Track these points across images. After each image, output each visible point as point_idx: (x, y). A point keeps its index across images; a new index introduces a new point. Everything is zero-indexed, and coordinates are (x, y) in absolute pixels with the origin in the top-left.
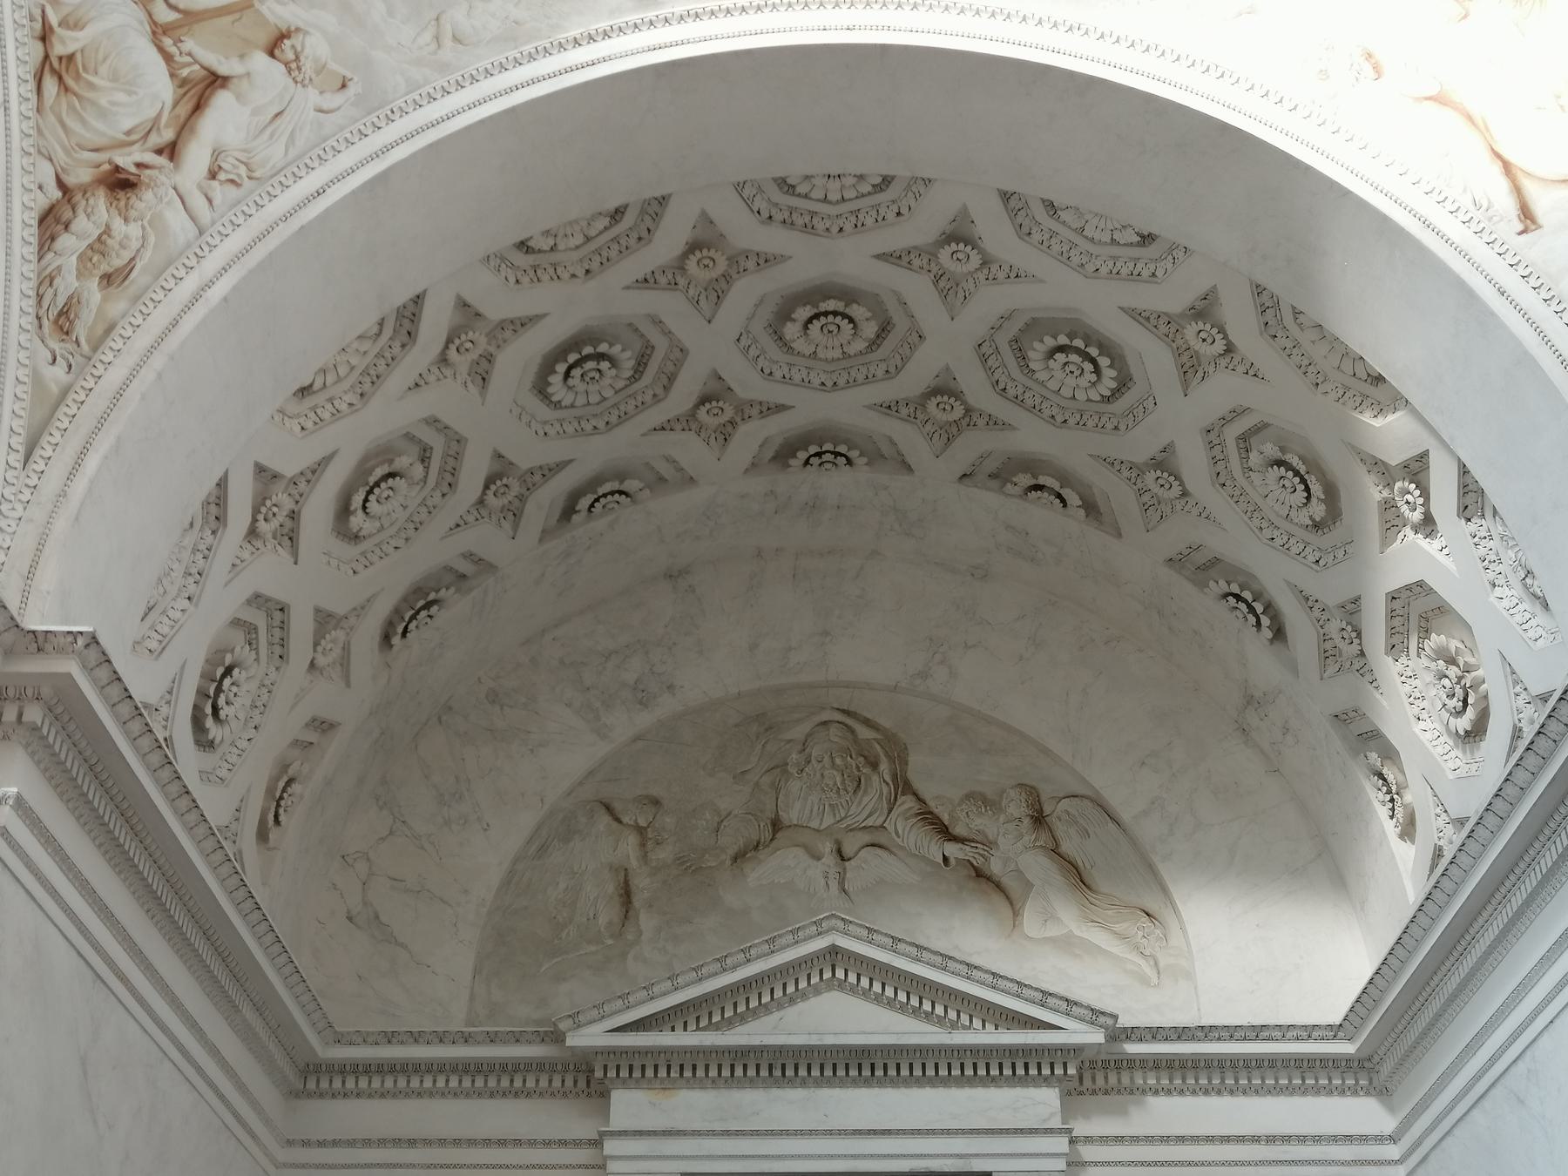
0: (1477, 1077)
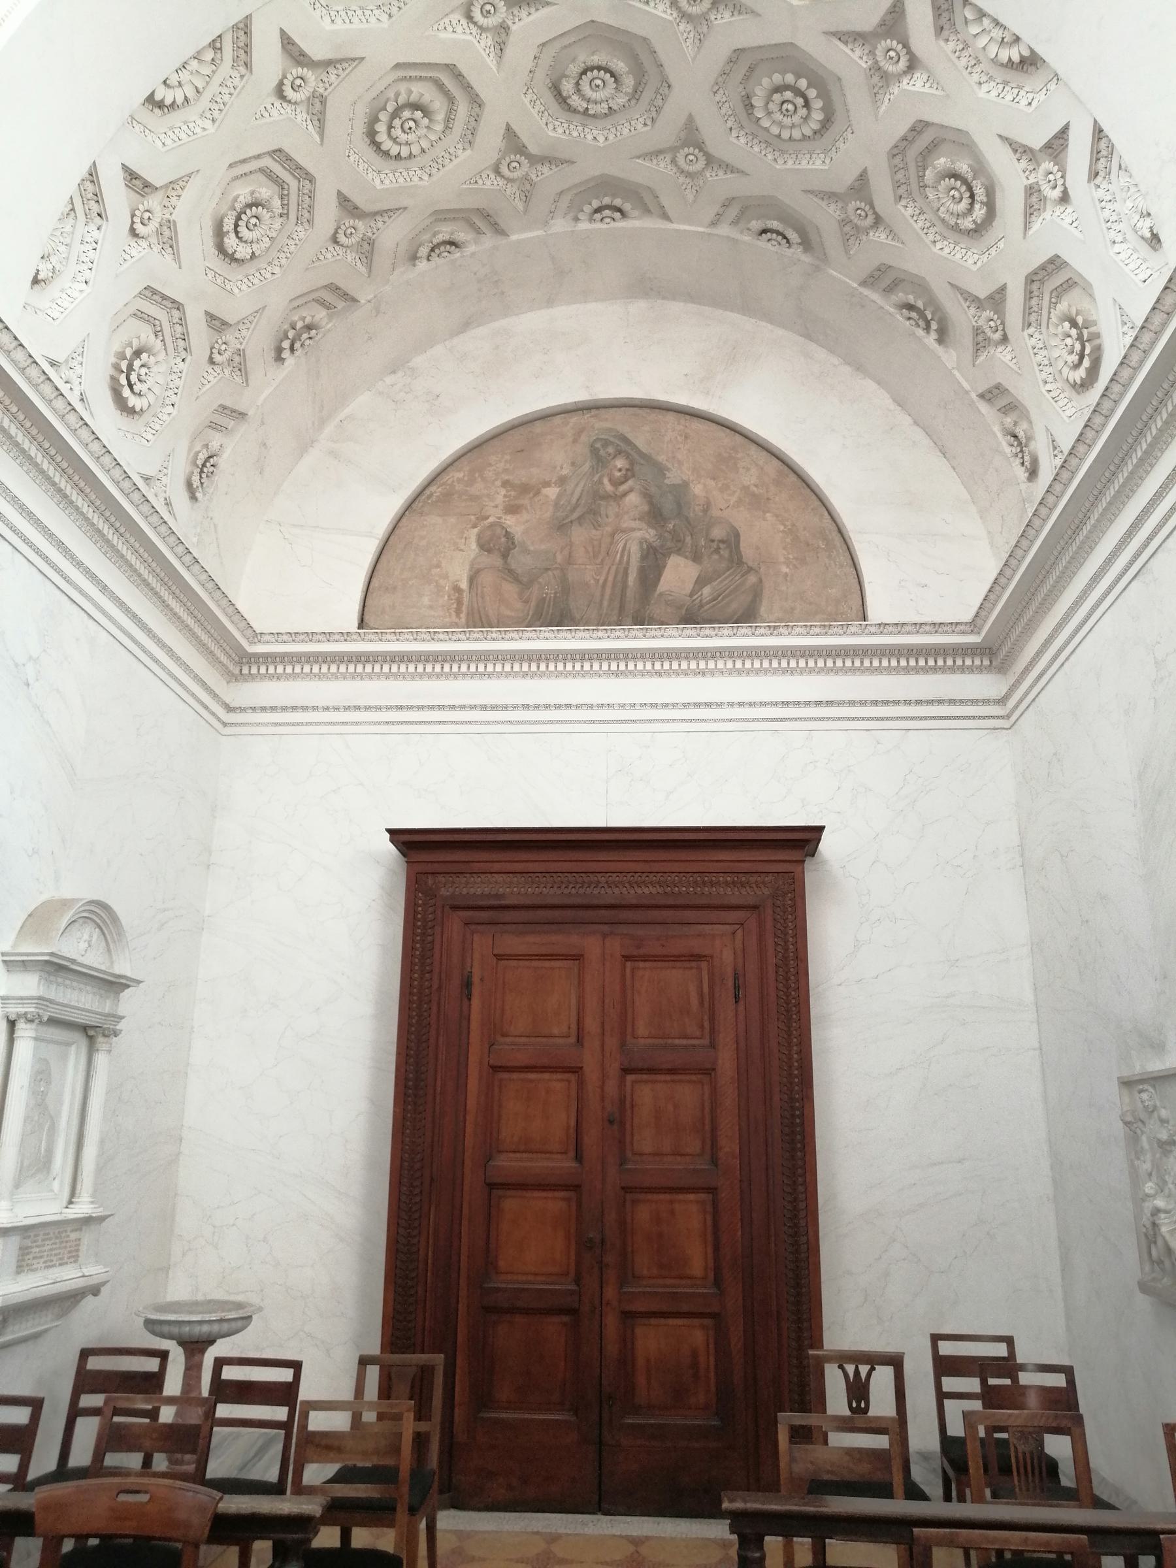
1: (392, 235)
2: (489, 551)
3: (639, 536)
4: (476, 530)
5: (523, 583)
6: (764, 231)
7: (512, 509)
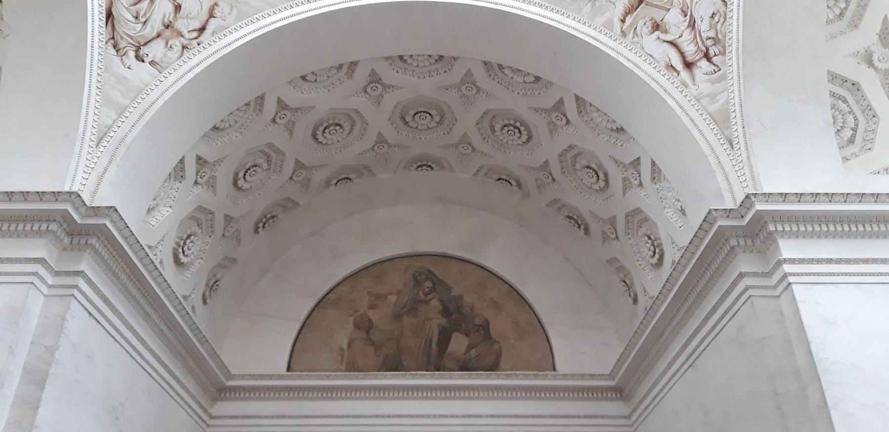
1: (318, 177)
2: (359, 329)
3: (436, 322)
4: (352, 318)
5: (377, 347)
6: (500, 179)
7: (372, 307)
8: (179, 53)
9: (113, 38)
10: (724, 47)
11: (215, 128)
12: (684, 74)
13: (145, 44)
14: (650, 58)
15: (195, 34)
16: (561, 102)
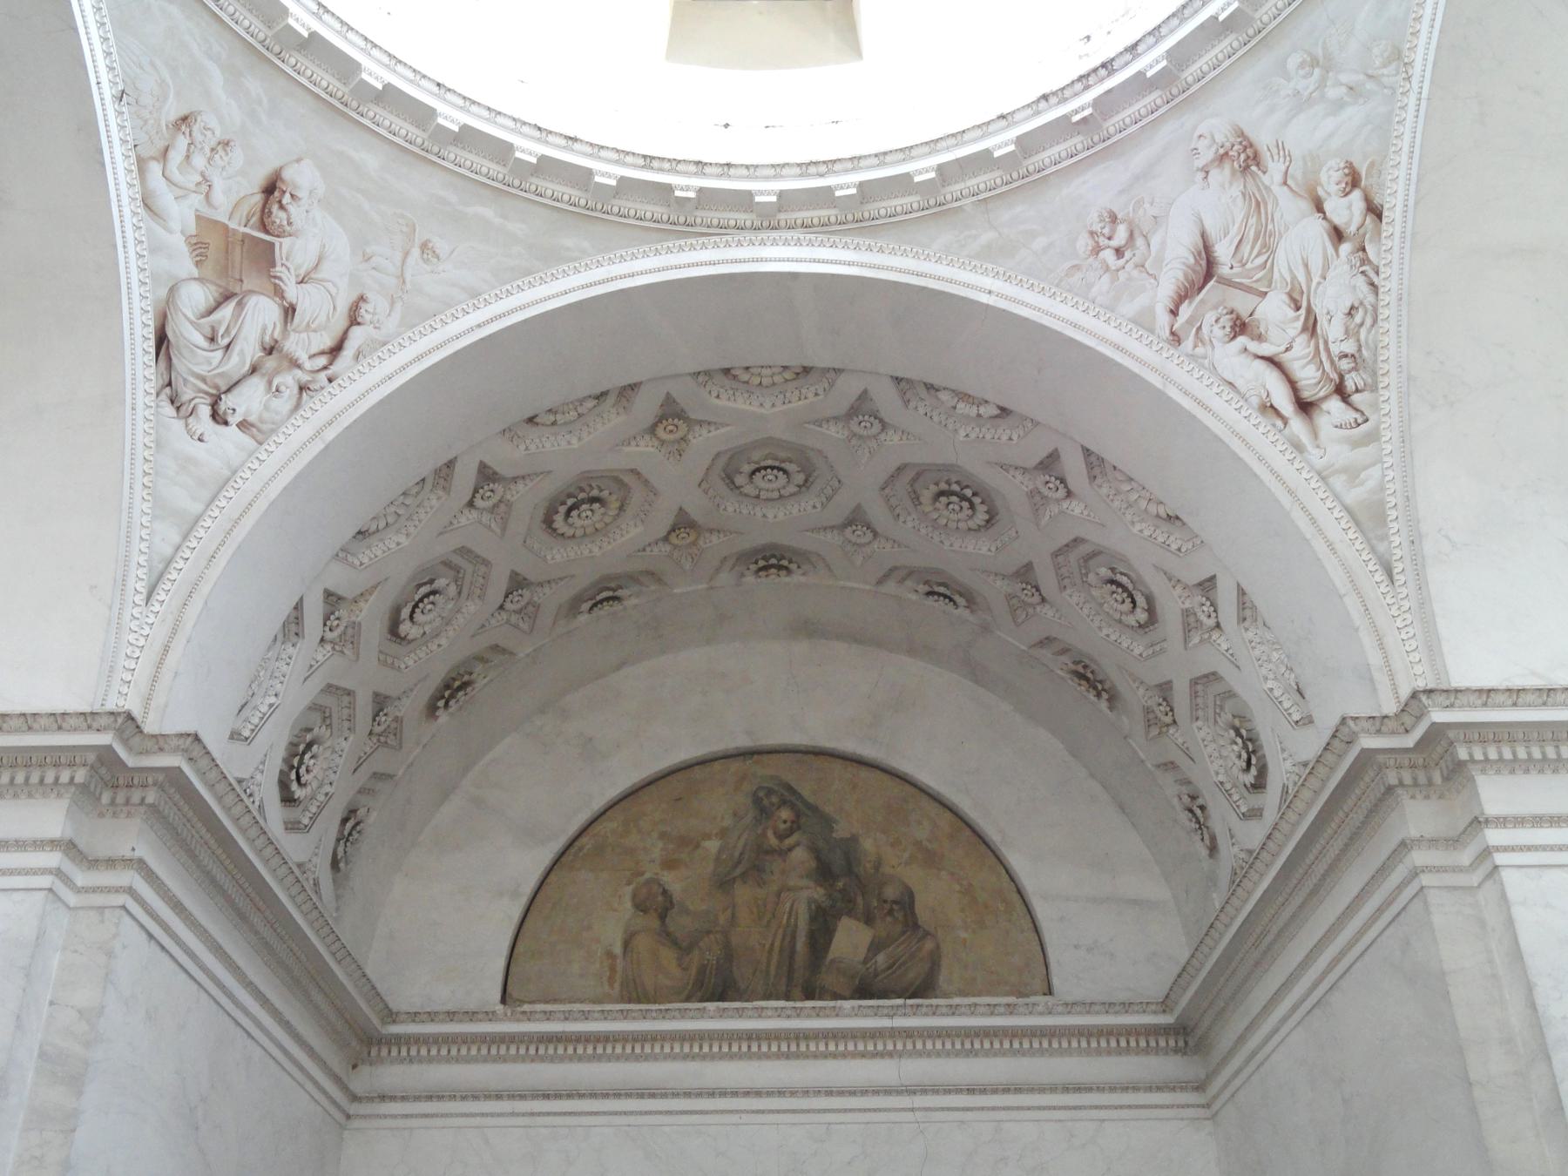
0: (1342, 953)
1: (551, 599)
2: (645, 911)
3: (806, 894)
4: (630, 889)
5: (683, 948)
7: (669, 864)
8: (294, 401)
9: (170, 384)
10: (1374, 374)
11: (360, 533)
12: (1297, 425)
13: (228, 390)
14: (1227, 389)
15: (323, 361)
16: (1054, 456)
